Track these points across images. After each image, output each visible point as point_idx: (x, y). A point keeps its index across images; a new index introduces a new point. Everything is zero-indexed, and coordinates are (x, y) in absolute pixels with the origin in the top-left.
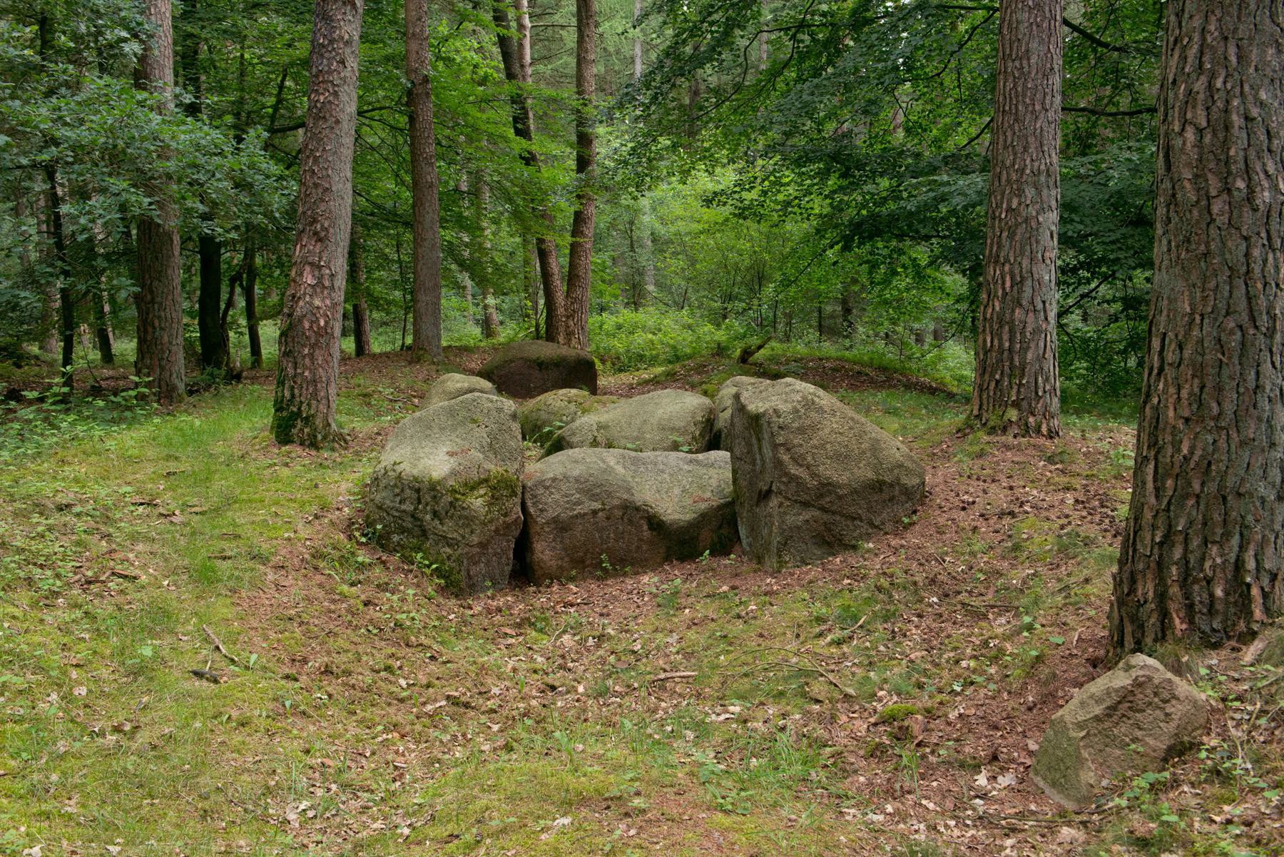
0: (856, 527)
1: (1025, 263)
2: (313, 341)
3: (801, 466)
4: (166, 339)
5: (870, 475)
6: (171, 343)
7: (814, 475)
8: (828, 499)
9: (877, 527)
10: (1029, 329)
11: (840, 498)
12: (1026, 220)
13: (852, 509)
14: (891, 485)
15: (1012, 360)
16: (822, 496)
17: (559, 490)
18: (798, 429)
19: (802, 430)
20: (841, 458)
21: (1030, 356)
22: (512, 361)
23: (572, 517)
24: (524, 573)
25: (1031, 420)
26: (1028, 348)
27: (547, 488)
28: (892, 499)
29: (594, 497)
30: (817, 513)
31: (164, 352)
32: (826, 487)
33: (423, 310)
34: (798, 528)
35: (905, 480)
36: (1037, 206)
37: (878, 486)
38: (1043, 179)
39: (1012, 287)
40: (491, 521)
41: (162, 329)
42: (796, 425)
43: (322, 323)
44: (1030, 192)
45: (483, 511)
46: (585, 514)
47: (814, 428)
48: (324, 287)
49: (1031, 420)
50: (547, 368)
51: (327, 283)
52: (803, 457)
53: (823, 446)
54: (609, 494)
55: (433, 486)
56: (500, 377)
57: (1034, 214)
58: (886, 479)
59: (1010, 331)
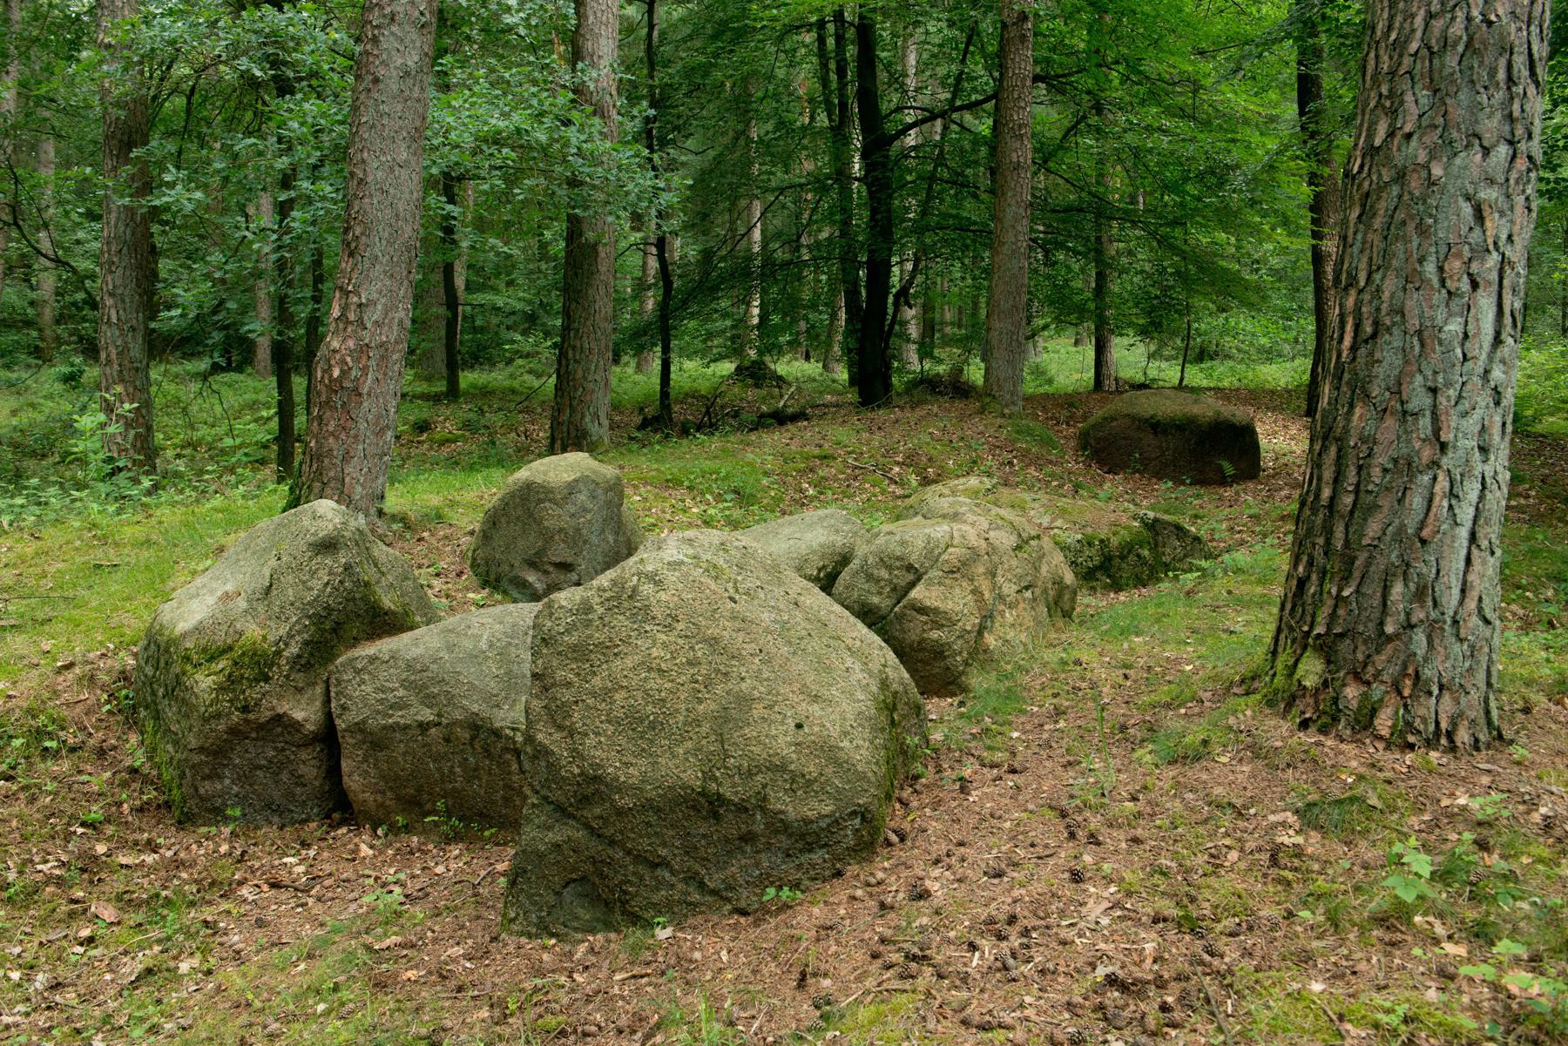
0: (660, 884)
1: (1390, 285)
2: (323, 398)
3: (560, 728)
4: (580, 373)
5: (692, 776)
6: (585, 378)
7: (576, 754)
8: (598, 811)
9: (714, 892)
10: (1381, 459)
11: (621, 812)
12: (1401, 177)
13: (644, 844)
14: (741, 808)
15: (1328, 533)
16: (585, 800)
17: (374, 677)
18: (574, 648)
19: (580, 652)
20: (643, 727)
21: (1373, 528)
22: (1113, 419)
23: (384, 728)
24: (340, 809)
25: (1352, 692)
26: (1373, 508)
27: (358, 672)
28: (748, 838)
29: (428, 700)
30: (580, 834)
31: (576, 390)
32: (593, 788)
33: (995, 342)
34: (541, 856)
35: (781, 802)
36: (1433, 138)
37: (710, 805)
38: (1451, 61)
39: (1354, 348)
40: (218, 716)
41: (576, 361)
42: (572, 639)
43: (336, 373)
44: (1416, 101)
45: (208, 698)
46: (407, 727)
47: (608, 650)
48: (348, 322)
49: (1352, 692)
50: (1165, 432)
51: (352, 317)
52: (565, 709)
53: (606, 694)
54: (451, 698)
55: (174, 642)
56: (1098, 441)
57: (1422, 157)
58: (726, 791)
59: (1340, 457)
